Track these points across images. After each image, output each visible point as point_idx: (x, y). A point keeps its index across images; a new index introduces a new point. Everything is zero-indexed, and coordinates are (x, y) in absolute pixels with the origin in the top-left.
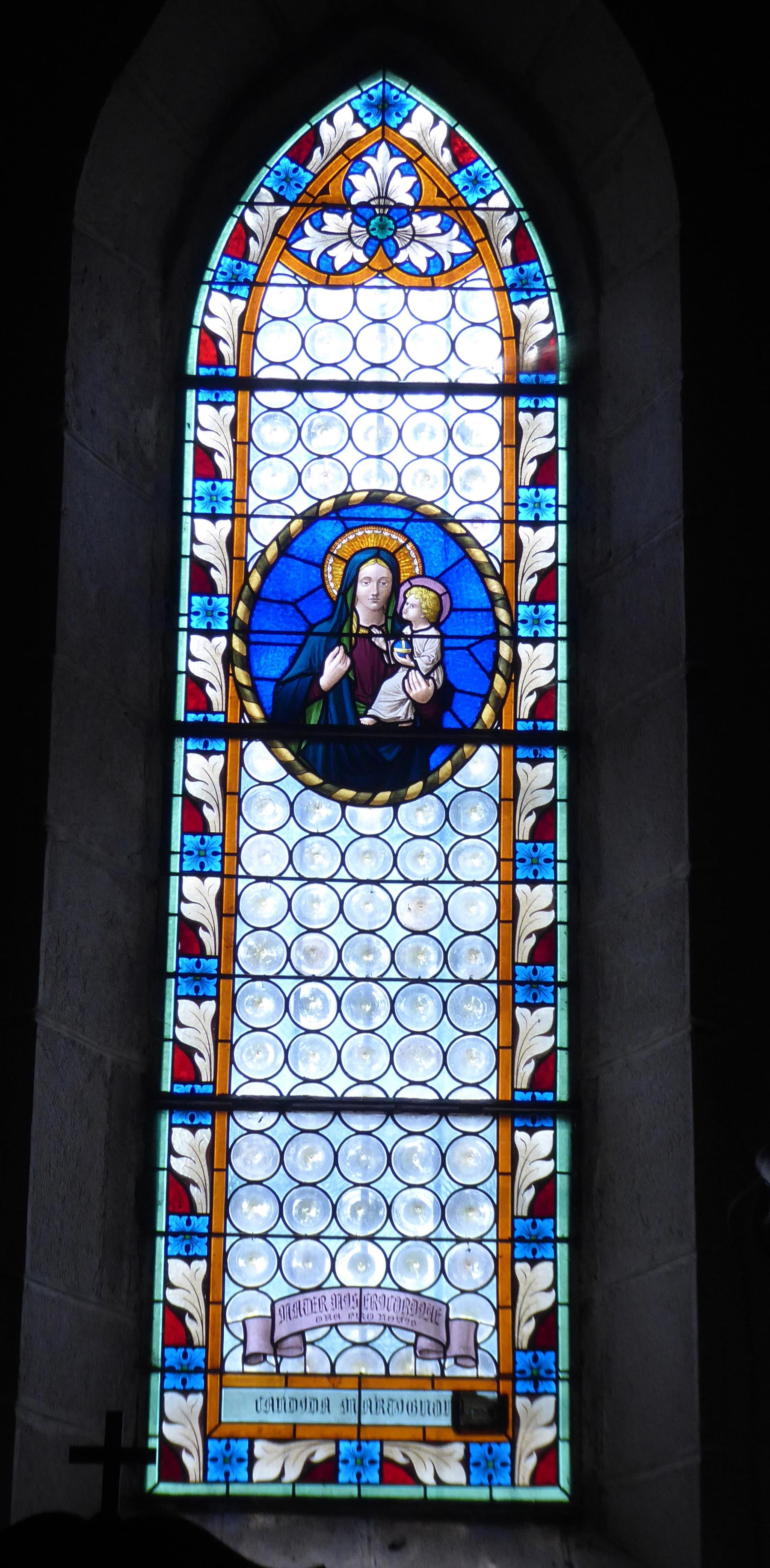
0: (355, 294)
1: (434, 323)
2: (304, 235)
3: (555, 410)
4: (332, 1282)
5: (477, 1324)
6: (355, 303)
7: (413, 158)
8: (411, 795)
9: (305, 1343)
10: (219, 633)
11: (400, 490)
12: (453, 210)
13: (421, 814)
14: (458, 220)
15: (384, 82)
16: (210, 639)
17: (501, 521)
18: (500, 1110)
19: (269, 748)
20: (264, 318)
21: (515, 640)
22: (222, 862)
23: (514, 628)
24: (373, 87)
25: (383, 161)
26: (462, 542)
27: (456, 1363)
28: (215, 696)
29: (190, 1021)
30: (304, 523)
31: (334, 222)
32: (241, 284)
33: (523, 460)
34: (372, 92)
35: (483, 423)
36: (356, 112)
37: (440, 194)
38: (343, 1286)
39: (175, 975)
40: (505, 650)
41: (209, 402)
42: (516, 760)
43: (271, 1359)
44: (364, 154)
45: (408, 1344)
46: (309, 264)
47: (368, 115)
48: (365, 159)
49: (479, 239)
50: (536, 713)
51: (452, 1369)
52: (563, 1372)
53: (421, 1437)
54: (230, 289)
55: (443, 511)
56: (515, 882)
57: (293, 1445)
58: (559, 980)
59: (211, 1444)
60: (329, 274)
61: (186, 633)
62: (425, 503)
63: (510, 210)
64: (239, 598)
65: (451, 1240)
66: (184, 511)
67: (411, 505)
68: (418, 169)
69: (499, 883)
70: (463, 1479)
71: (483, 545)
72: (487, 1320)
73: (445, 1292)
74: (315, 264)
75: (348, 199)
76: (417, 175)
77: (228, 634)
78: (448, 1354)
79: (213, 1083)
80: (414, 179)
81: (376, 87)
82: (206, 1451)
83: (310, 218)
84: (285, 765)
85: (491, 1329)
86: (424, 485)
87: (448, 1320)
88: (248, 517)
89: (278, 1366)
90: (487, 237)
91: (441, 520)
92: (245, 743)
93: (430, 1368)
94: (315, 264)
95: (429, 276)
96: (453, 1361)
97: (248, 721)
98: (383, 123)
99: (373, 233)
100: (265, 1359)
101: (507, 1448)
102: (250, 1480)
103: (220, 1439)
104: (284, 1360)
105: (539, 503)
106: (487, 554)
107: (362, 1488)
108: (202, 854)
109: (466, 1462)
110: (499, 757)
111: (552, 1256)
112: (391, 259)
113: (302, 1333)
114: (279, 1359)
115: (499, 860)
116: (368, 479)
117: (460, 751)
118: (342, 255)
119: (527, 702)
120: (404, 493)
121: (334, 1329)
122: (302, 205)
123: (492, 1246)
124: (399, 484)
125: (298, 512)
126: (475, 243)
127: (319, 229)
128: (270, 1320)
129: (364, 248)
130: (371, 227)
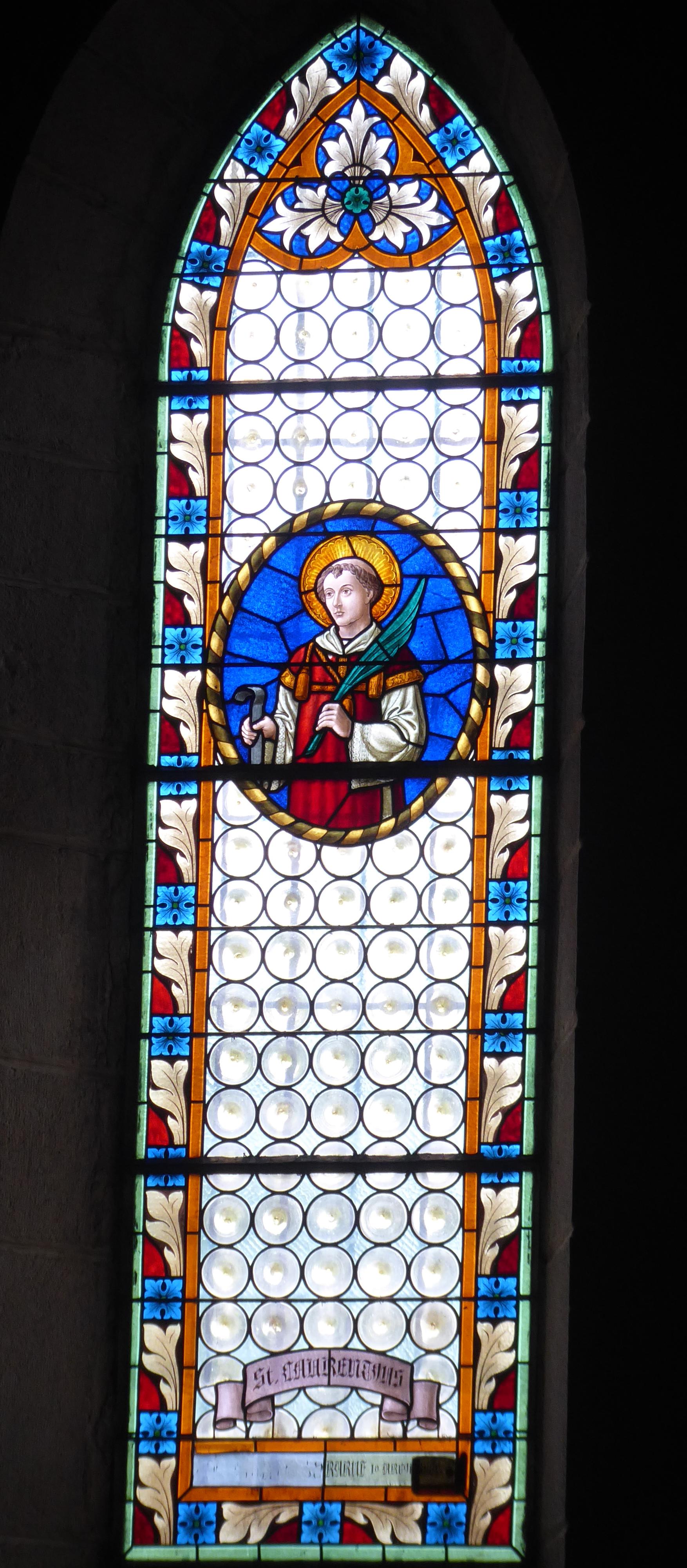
0: (332, 278)
1: (463, 305)
2: (277, 215)
3: (539, 402)
4: (302, 1345)
5: (439, 1385)
6: (279, 290)
7: (388, 116)
8: (381, 834)
9: (274, 1407)
10: (194, 667)
11: (378, 499)
12: (435, 177)
13: (394, 852)
14: (436, 187)
15: (358, 28)
16: (184, 673)
17: (481, 530)
18: (466, 1164)
19: (243, 789)
20: (237, 313)
21: (490, 663)
22: (195, 914)
23: (491, 650)
24: (347, 34)
25: (357, 121)
26: (440, 556)
27: (418, 1424)
28: (189, 735)
29: (162, 1081)
30: (277, 541)
31: (308, 197)
32: (214, 274)
33: (505, 460)
34: (346, 40)
35: (462, 418)
36: (329, 64)
37: (417, 157)
38: (311, 1348)
39: (149, 1036)
40: (481, 672)
41: (182, 411)
42: (490, 792)
43: (241, 1424)
44: (337, 115)
45: (373, 1405)
46: (282, 247)
47: (342, 68)
48: (339, 121)
49: (455, 208)
50: (512, 742)
51: (416, 1432)
52: (520, 1431)
53: (383, 1499)
54: (201, 280)
55: (421, 521)
56: (487, 924)
57: (263, 1506)
58: (528, 1027)
59: (182, 1509)
60: (302, 257)
61: (159, 669)
62: (402, 512)
63: (493, 172)
64: (213, 629)
65: (451, 1299)
66: (157, 533)
67: (390, 514)
68: (395, 131)
69: (472, 925)
70: (418, 1539)
71: (461, 556)
72: (449, 1380)
73: (406, 1352)
74: (287, 247)
75: (322, 171)
76: (393, 136)
77: (202, 668)
78: (412, 1417)
79: (187, 1146)
80: (389, 140)
81: (348, 34)
82: (176, 1514)
83: (282, 194)
84: (258, 805)
85: (453, 1389)
86: (403, 492)
87: (412, 1381)
88: (224, 535)
89: (248, 1431)
90: (468, 206)
91: (419, 531)
92: (218, 783)
93: (396, 1430)
94: (287, 247)
95: (406, 255)
96: (416, 1422)
97: (221, 763)
98: (358, 77)
99: (348, 207)
100: (235, 1425)
101: (462, 1509)
102: (217, 1542)
103: (189, 1503)
104: (254, 1425)
105: (190, 521)
106: (464, 566)
107: (325, 1548)
108: (176, 904)
109: (423, 1522)
110: (474, 789)
111: (515, 1315)
112: (367, 235)
113: (271, 1398)
114: (248, 1425)
115: (472, 901)
116: (351, 486)
117: (432, 787)
118: (317, 236)
119: (504, 730)
120: (382, 502)
121: (302, 1393)
122: (272, 180)
123: (456, 1305)
124: (378, 492)
125: (272, 530)
126: (454, 213)
127: (291, 207)
128: (241, 1386)
129: (338, 226)
130: (346, 200)
